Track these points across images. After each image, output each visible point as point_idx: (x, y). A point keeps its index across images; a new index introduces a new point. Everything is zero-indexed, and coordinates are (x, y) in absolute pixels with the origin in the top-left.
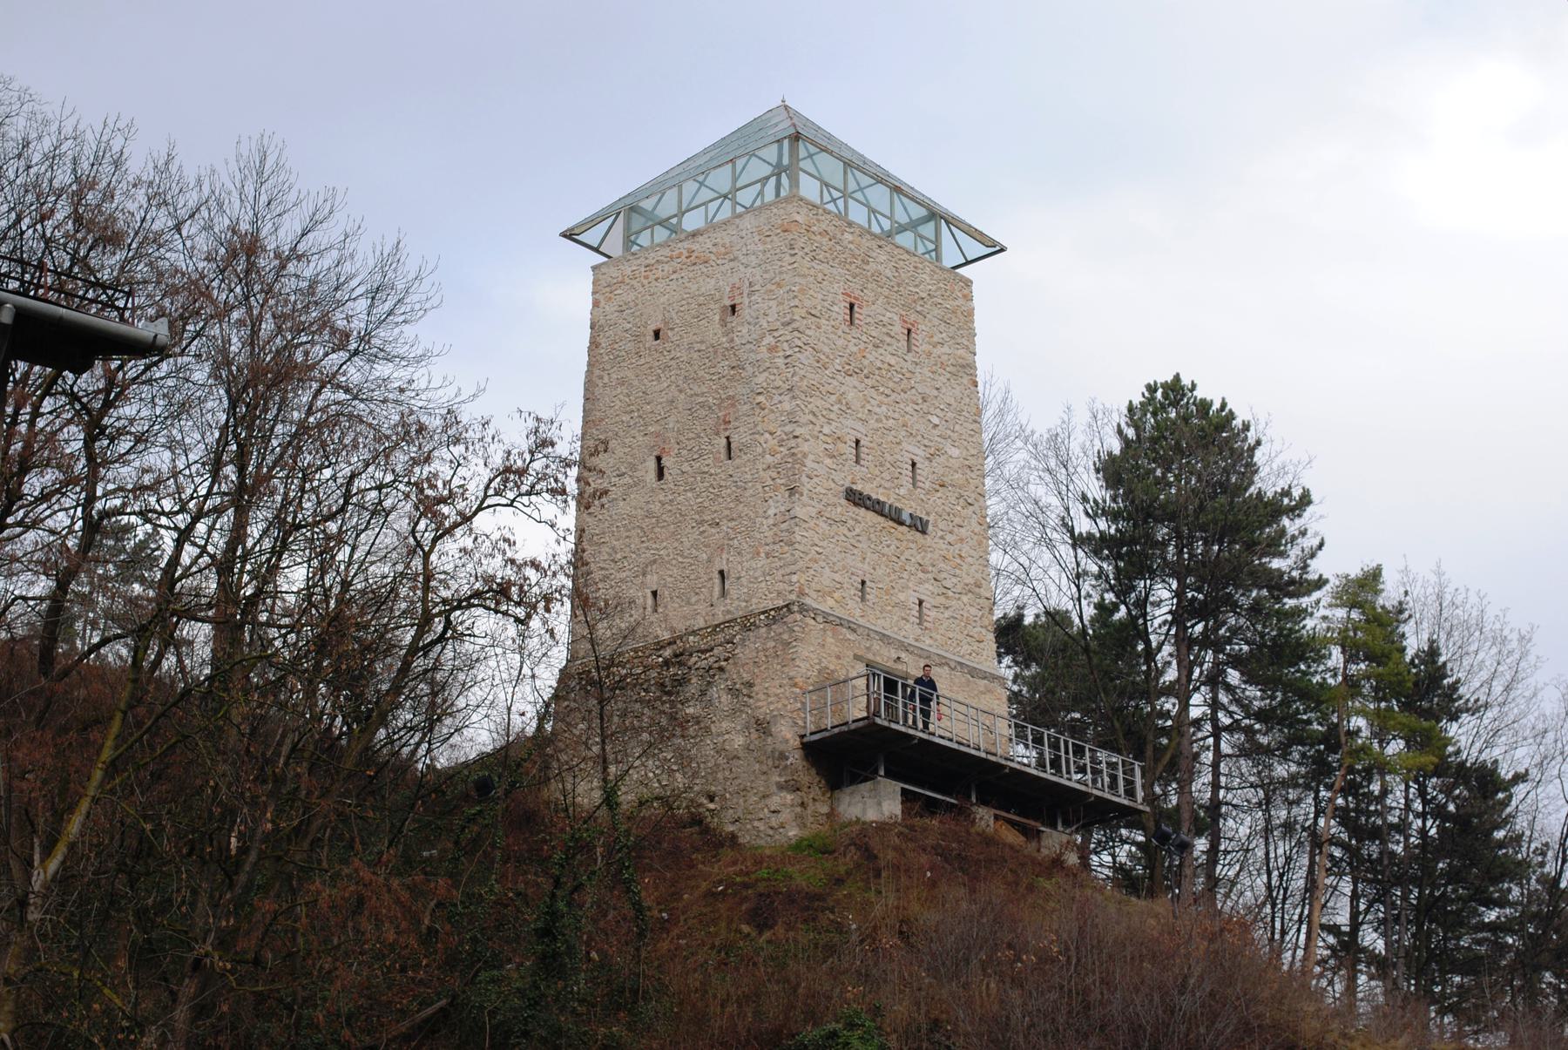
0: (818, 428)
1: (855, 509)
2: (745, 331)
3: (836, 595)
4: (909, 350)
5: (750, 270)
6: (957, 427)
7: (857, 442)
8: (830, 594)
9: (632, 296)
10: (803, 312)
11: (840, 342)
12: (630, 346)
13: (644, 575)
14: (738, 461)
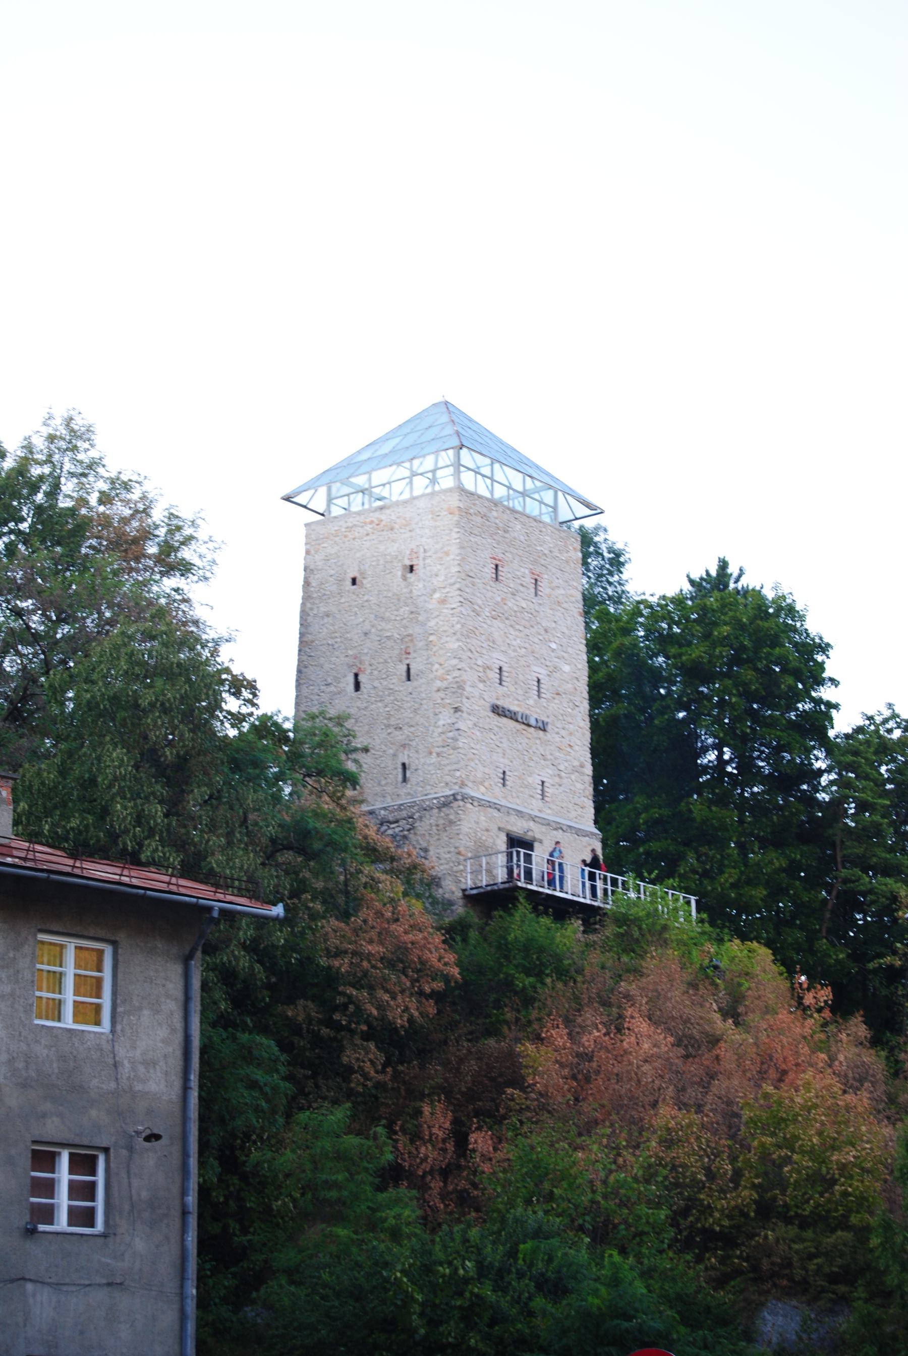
2: (421, 586)
4: (536, 595)
5: (424, 539)
6: (569, 650)
7: (500, 669)
8: (482, 783)
12: (334, 588)
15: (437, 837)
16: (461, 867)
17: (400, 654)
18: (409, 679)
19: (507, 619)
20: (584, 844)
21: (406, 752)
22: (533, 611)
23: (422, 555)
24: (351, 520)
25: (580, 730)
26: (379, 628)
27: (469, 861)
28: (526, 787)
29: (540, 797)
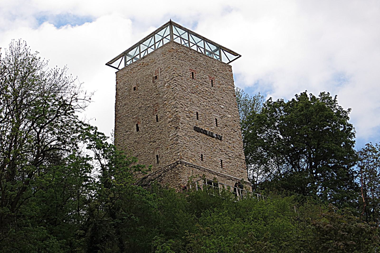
0: (184, 109)
2: (160, 83)
3: (193, 159)
4: (212, 86)
5: (160, 65)
6: (230, 109)
8: (191, 159)
11: (190, 83)
14: (160, 122)
24: (132, 66)
25: (238, 141)
26: (145, 104)
28: (213, 162)
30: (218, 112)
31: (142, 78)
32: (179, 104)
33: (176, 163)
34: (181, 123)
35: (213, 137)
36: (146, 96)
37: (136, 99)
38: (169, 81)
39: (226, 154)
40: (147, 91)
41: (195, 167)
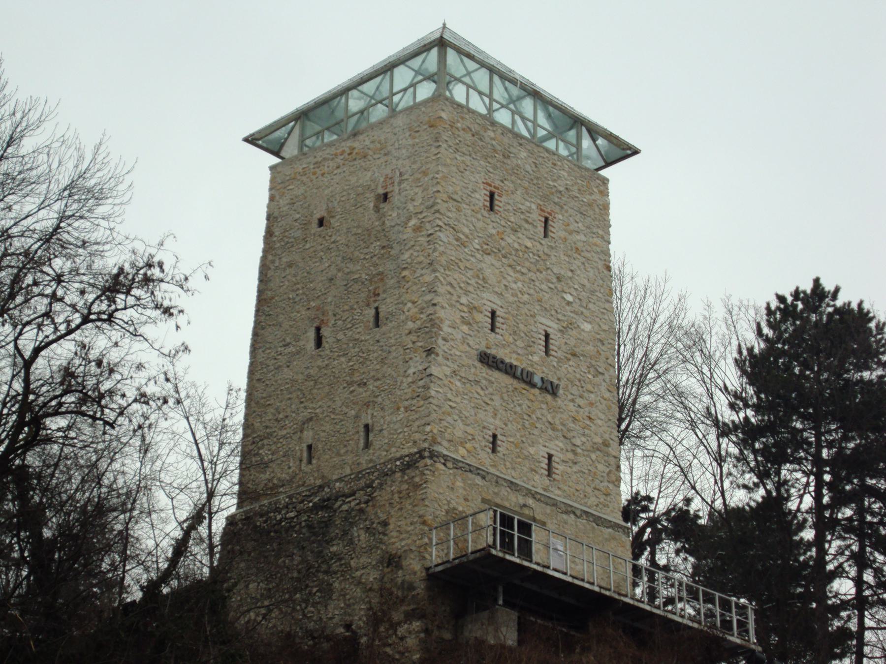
0: (455, 298)
1: (490, 372)
2: (394, 215)
3: (468, 445)
4: (546, 236)
5: (400, 162)
6: (591, 306)
7: (493, 313)
8: (462, 444)
9: (301, 191)
10: (445, 196)
12: (298, 234)
13: (302, 431)
15: (398, 506)
16: (426, 540)
17: (368, 297)
18: (377, 325)
19: (505, 257)
20: (606, 536)
21: (369, 411)
22: (541, 253)
23: (397, 180)
24: (320, 154)
25: (604, 402)
26: (347, 270)
27: (434, 532)
29: (547, 473)
30: (553, 312)
31: (345, 193)
32: (444, 282)
33: (417, 456)
34: (445, 339)
35: (534, 386)
36: (352, 249)
37: (322, 253)
38: (421, 213)
39: (564, 437)
40: (356, 234)
41: (470, 471)
